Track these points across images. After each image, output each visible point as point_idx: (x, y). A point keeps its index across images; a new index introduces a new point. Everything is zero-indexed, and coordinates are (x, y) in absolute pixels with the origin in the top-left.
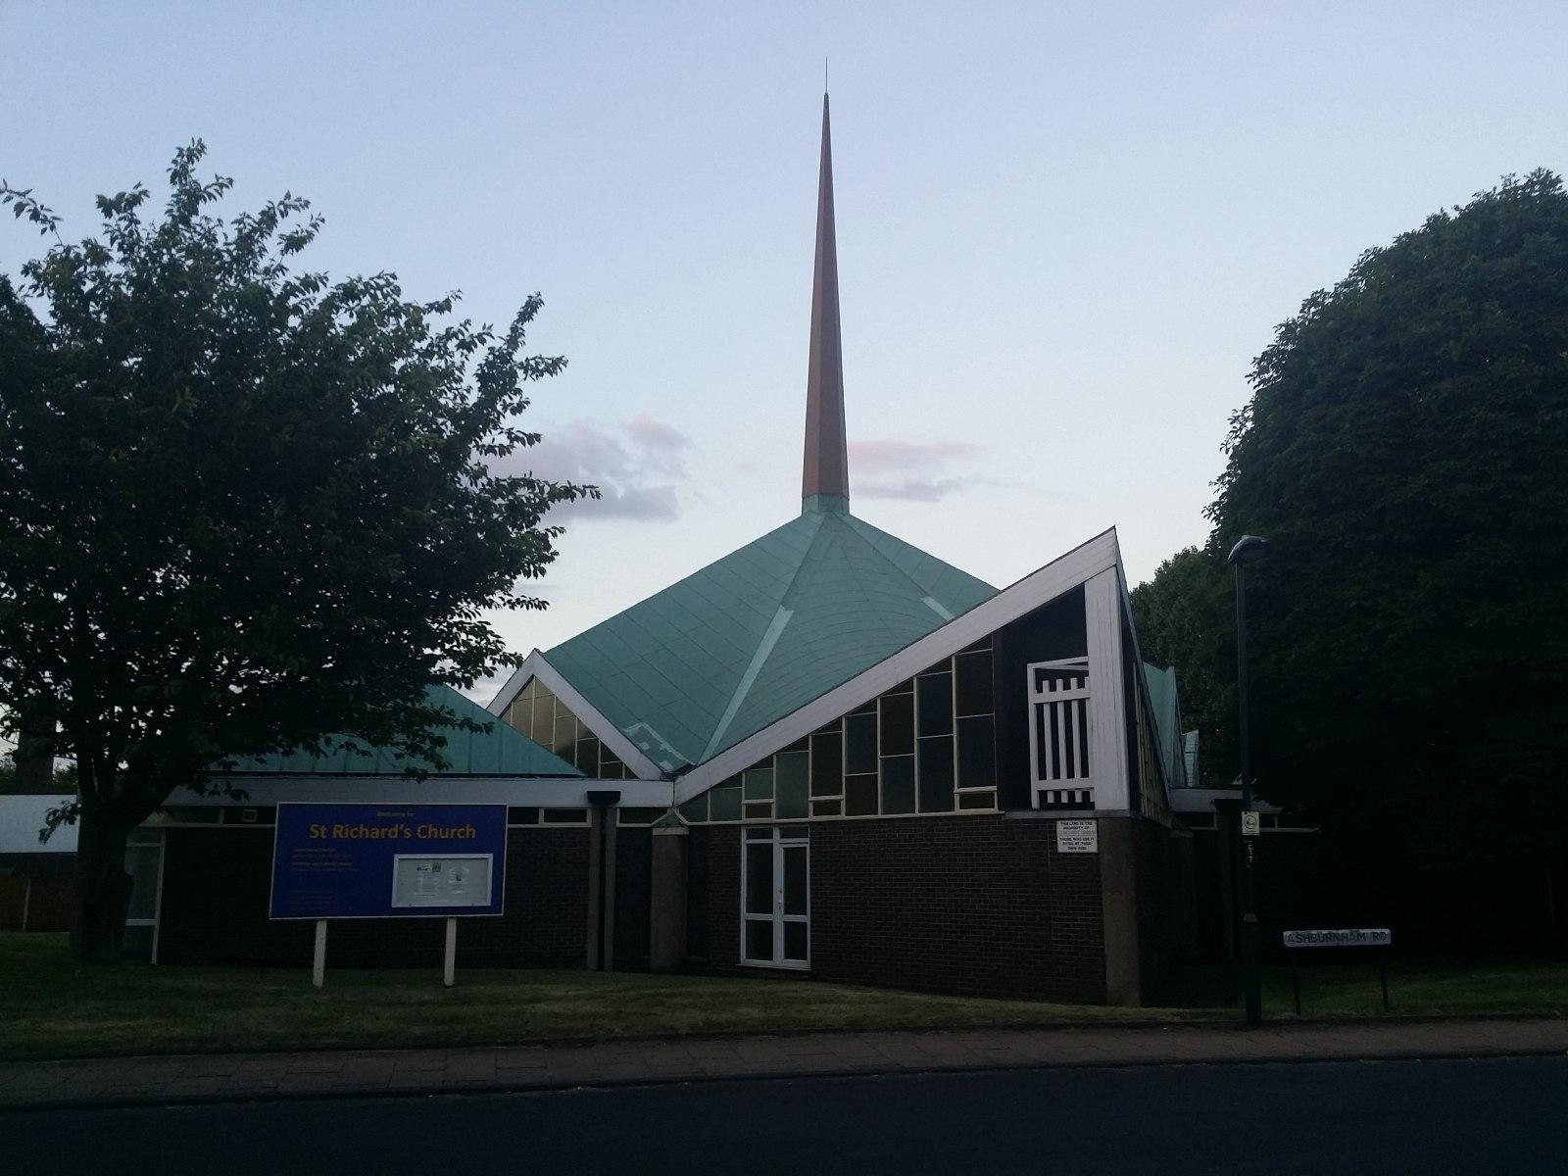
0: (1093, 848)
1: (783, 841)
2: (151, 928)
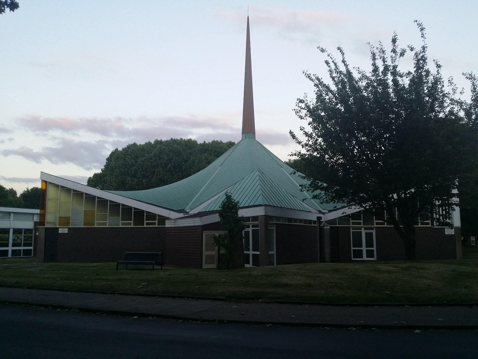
0: (453, 233)
1: (365, 231)
2: (31, 250)
